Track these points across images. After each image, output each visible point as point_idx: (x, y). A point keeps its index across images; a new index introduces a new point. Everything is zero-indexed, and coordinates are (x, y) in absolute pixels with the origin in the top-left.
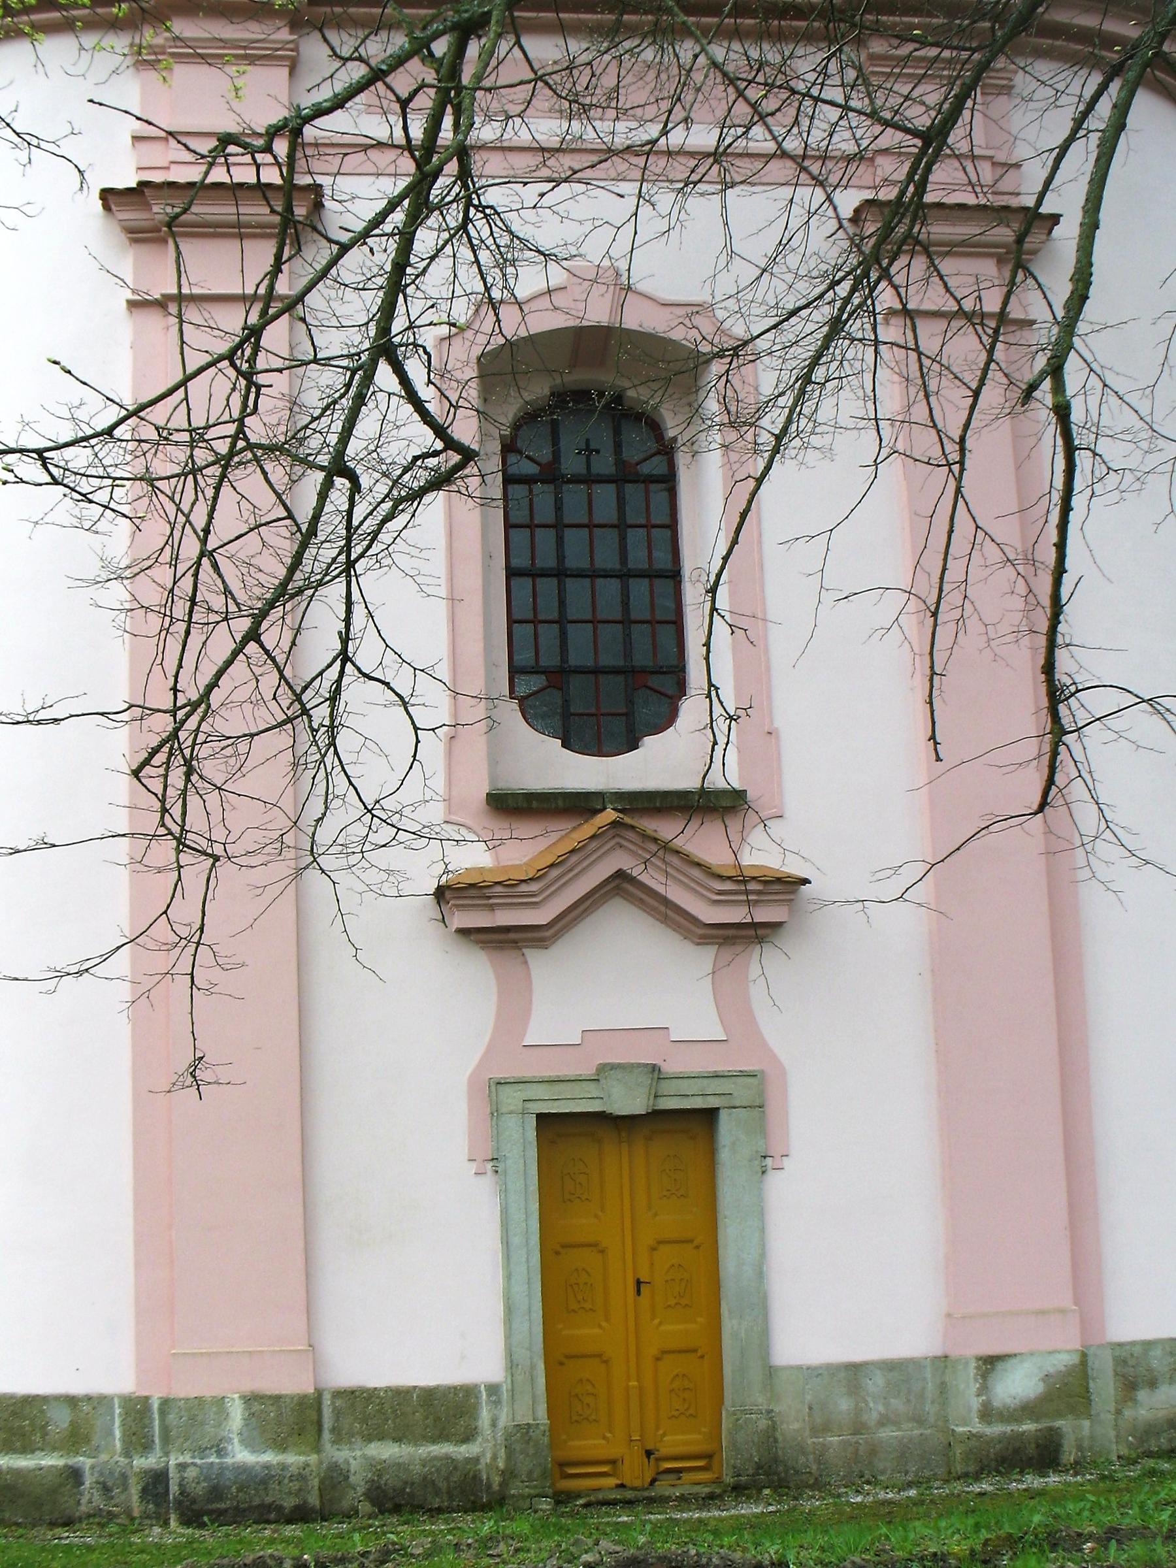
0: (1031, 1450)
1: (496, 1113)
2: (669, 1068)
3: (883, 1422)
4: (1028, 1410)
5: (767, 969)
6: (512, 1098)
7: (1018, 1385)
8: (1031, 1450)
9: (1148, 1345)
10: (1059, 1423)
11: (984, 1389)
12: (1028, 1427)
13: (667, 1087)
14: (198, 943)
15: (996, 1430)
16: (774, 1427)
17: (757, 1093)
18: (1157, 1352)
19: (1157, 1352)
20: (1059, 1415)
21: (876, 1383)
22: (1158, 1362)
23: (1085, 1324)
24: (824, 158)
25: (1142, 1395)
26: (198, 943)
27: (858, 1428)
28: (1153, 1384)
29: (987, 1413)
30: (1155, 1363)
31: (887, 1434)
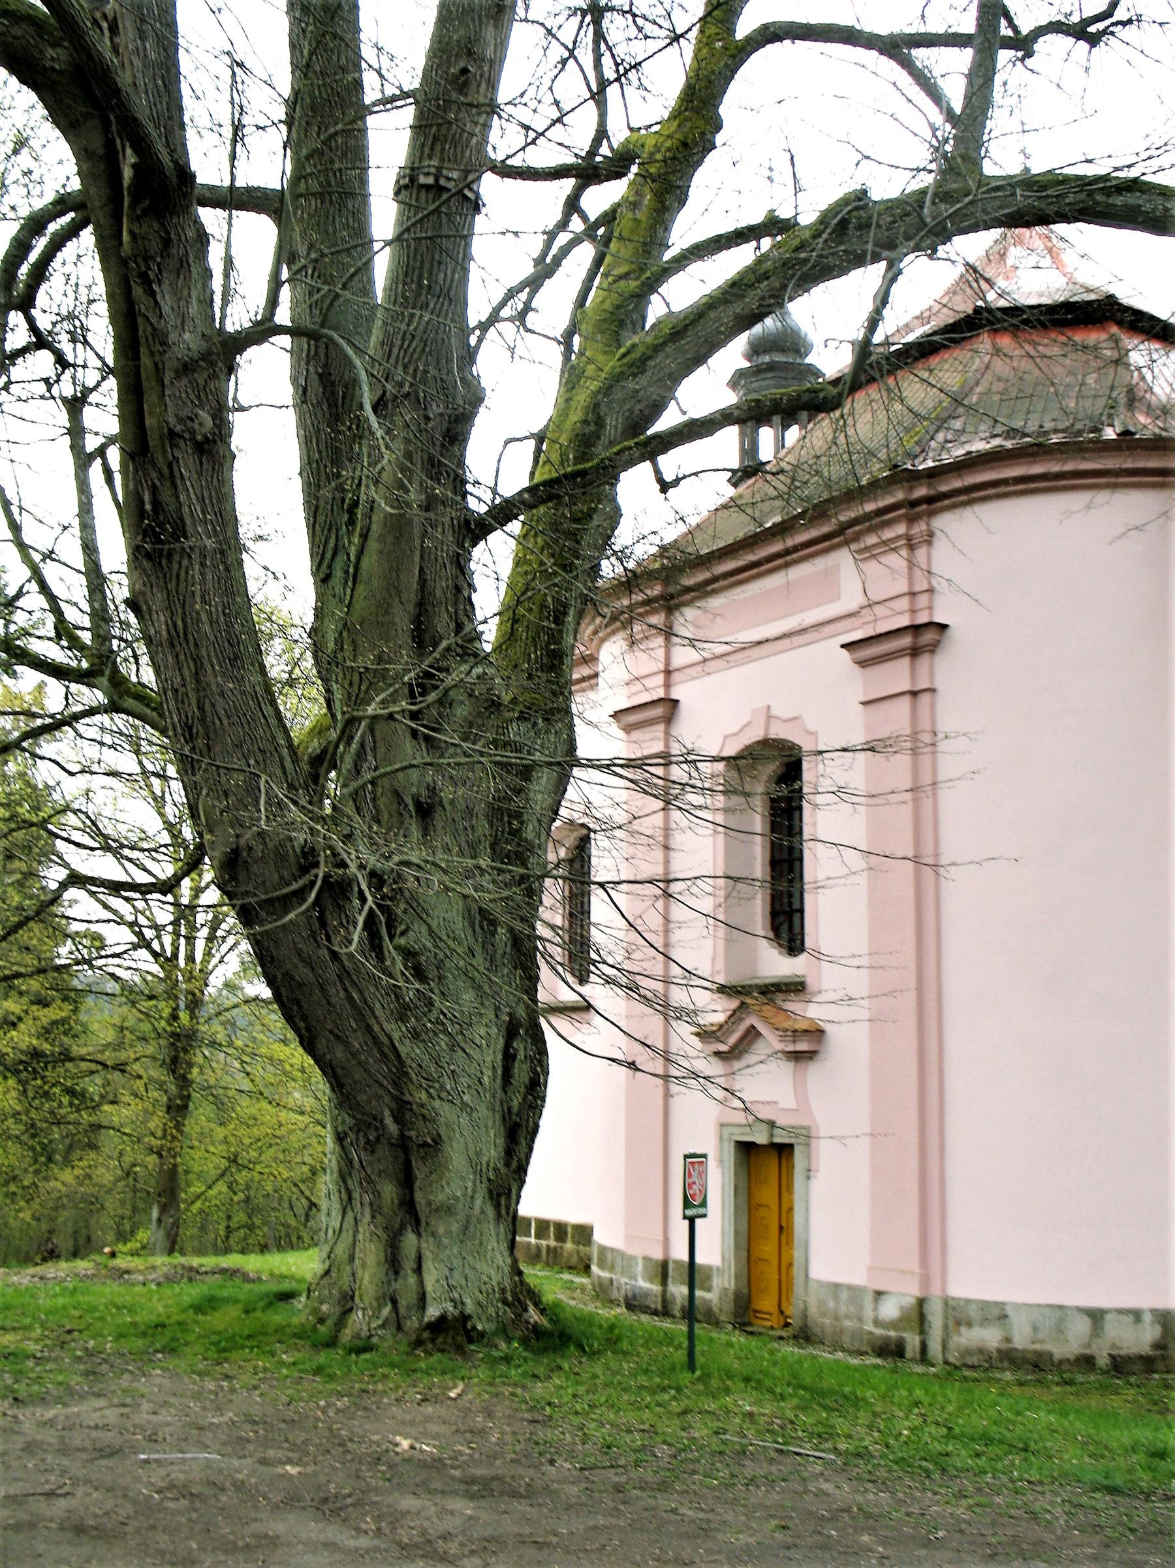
0: (893, 1347)
1: (721, 1139)
2: (779, 1123)
3: (847, 1317)
4: (893, 1325)
5: (814, 1072)
6: (727, 1131)
7: (890, 1310)
8: (893, 1347)
9: (968, 1301)
10: (905, 1335)
11: (875, 1309)
12: (892, 1333)
13: (777, 1131)
14: (101, 744)
15: (879, 1332)
16: (806, 1309)
17: (807, 1135)
18: (974, 1307)
19: (974, 1307)
20: (904, 1330)
21: (844, 1295)
22: (973, 1312)
23: (925, 1279)
24: (793, 479)
25: (963, 1329)
26: (101, 744)
27: (837, 1318)
28: (969, 1324)
29: (877, 1322)
30: (972, 1313)
31: (847, 1323)
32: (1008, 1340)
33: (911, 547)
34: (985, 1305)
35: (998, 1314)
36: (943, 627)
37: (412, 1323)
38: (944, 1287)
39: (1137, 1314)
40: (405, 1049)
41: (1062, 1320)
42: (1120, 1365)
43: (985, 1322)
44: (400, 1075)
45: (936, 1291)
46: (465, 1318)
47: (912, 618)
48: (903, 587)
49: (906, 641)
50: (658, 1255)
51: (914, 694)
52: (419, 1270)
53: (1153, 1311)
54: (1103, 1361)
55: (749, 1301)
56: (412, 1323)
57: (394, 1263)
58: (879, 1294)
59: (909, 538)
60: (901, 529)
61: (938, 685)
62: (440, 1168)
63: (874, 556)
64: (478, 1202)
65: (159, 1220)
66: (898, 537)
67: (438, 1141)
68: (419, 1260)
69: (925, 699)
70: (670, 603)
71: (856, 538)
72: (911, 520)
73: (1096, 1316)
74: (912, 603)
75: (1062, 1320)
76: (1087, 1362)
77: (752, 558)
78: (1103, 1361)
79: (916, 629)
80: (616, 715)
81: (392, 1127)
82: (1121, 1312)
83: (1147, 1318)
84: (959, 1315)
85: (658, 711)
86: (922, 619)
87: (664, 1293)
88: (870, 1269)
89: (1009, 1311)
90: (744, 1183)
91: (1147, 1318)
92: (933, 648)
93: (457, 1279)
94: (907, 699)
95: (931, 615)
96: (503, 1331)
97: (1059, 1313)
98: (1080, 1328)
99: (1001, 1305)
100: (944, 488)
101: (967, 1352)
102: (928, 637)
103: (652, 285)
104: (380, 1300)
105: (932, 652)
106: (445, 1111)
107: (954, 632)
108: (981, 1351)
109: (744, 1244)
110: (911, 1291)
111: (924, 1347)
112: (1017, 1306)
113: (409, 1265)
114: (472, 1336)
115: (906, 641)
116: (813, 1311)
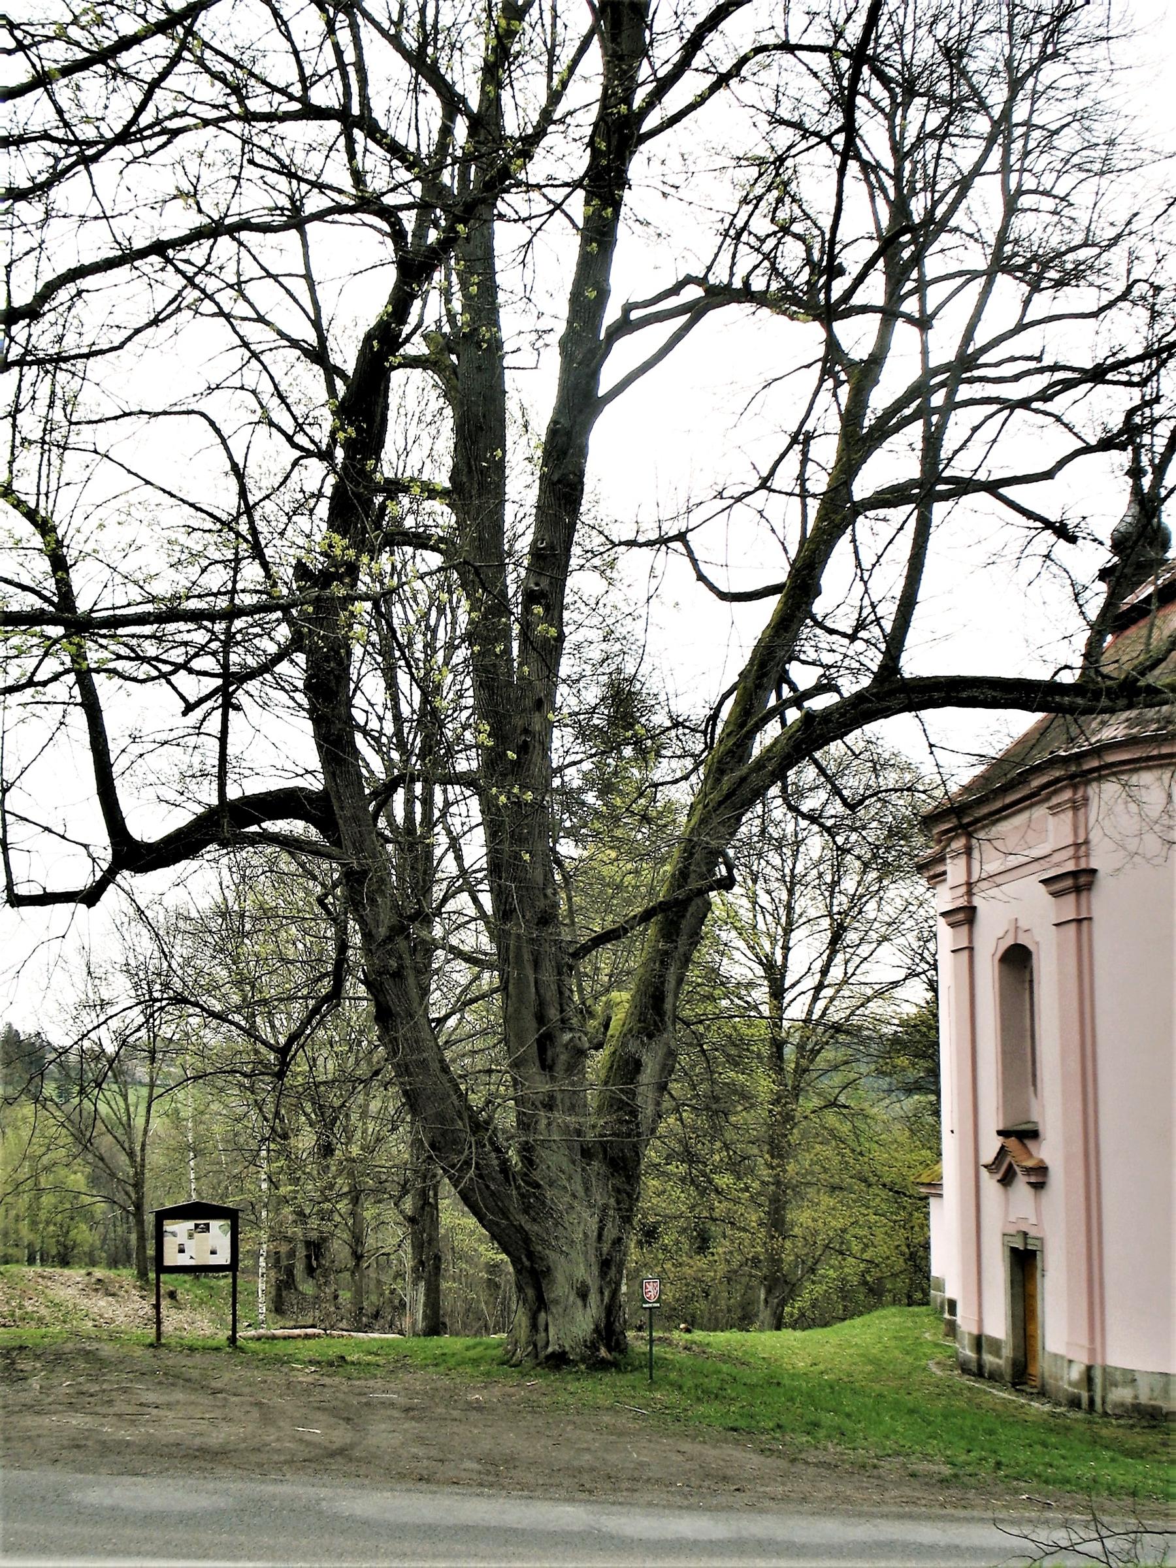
15: (1070, 1389)
22: (1119, 1377)
23: (1092, 1352)
32: (1136, 1397)
33: (1075, 809)
34: (1125, 1371)
35: (1130, 1378)
37: (542, 1355)
38: (1104, 1358)
40: (527, 1227)
44: (527, 1240)
45: (1099, 1361)
46: (564, 1353)
47: (1077, 864)
48: (1070, 841)
49: (1069, 882)
50: (975, 1332)
51: (1079, 921)
52: (546, 1330)
55: (1026, 1367)
56: (542, 1355)
57: (534, 1326)
58: (1070, 1361)
61: (1095, 914)
62: (552, 1282)
64: (571, 1299)
66: (1066, 802)
67: (549, 1268)
68: (547, 1325)
69: (1085, 923)
70: (967, 830)
71: (1048, 798)
72: (1075, 788)
74: (1077, 851)
75: (1167, 1384)
77: (1008, 800)
81: (527, 1263)
84: (1112, 1377)
86: (1083, 866)
87: (979, 1360)
88: (1068, 1344)
89: (1137, 1376)
90: (1019, 1277)
92: (1089, 886)
93: (561, 1335)
95: (1088, 862)
96: (583, 1360)
97: (1164, 1379)
100: (1086, 767)
101: (1116, 1405)
102: (1083, 880)
103: (751, 736)
104: (528, 1343)
105: (1089, 889)
106: (552, 1256)
107: (1100, 874)
108: (1122, 1405)
109: (1020, 1324)
111: (1092, 1401)
113: (541, 1328)
114: (568, 1362)
115: (1069, 882)
116: (1046, 1374)
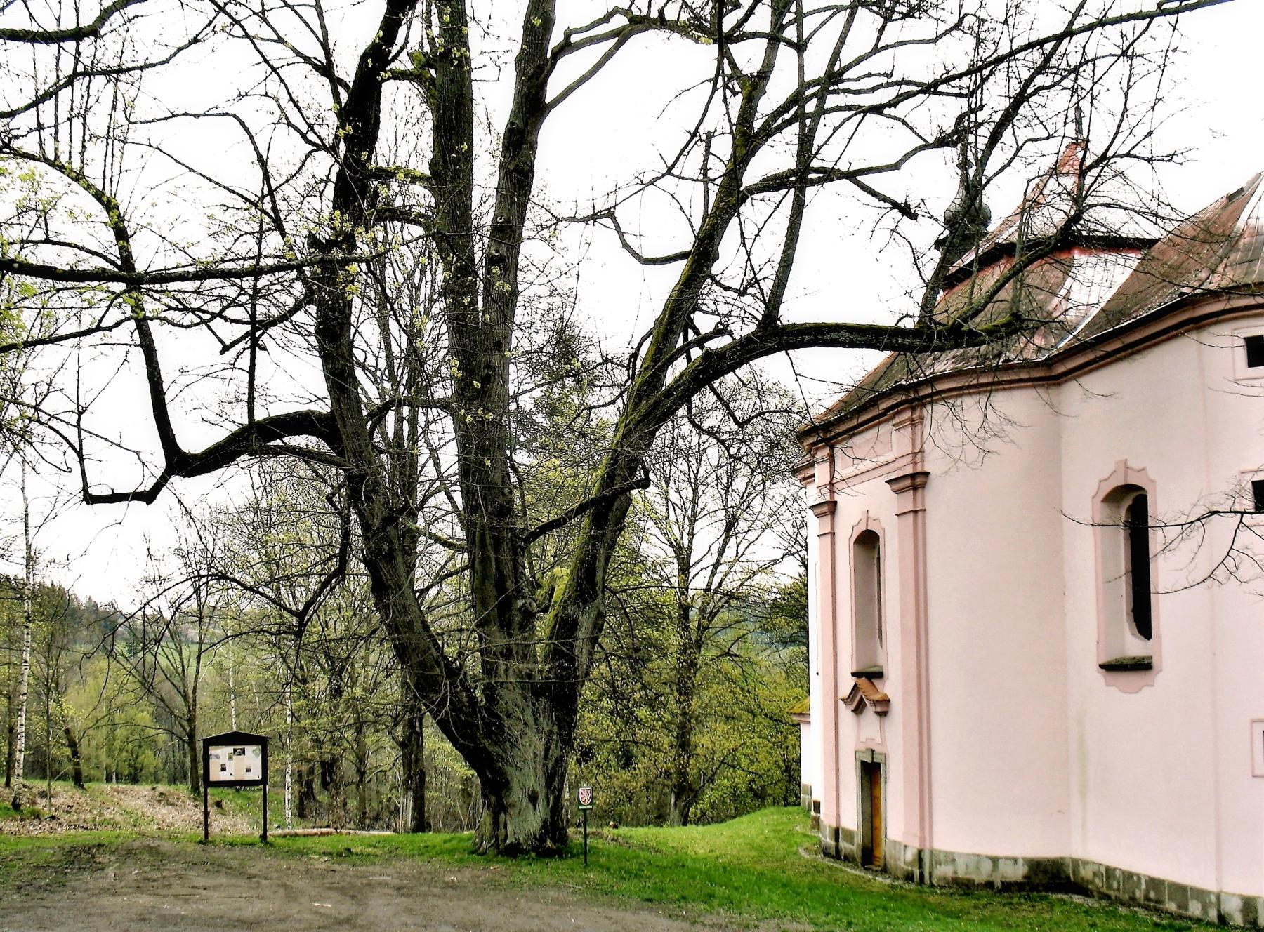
15: (906, 867)
22: (942, 857)
23: (922, 839)
32: (955, 872)
33: (913, 425)
34: (947, 853)
35: (951, 858)
36: (927, 474)
37: (502, 846)
39: (1015, 860)
41: (978, 862)
42: (1008, 887)
43: (946, 862)
45: (928, 846)
46: (519, 844)
49: (908, 482)
51: (916, 512)
52: (505, 827)
53: (1024, 859)
54: (998, 884)
56: (502, 846)
57: (496, 824)
59: (912, 420)
60: (907, 415)
63: (943, 399)
65: (675, 804)
66: (905, 421)
69: (920, 514)
70: (830, 443)
73: (995, 860)
76: (989, 885)
78: (998, 884)
79: (913, 476)
80: (811, 507)
82: (1007, 858)
83: (1020, 862)
84: (936, 859)
85: (825, 509)
86: (919, 469)
91: (1020, 862)
92: (923, 485)
93: (517, 830)
94: (911, 515)
98: (987, 867)
99: (952, 853)
102: (919, 480)
104: (491, 838)
107: (932, 476)
109: (868, 818)
110: (914, 845)
112: (961, 855)
113: (502, 826)
115: (908, 482)
